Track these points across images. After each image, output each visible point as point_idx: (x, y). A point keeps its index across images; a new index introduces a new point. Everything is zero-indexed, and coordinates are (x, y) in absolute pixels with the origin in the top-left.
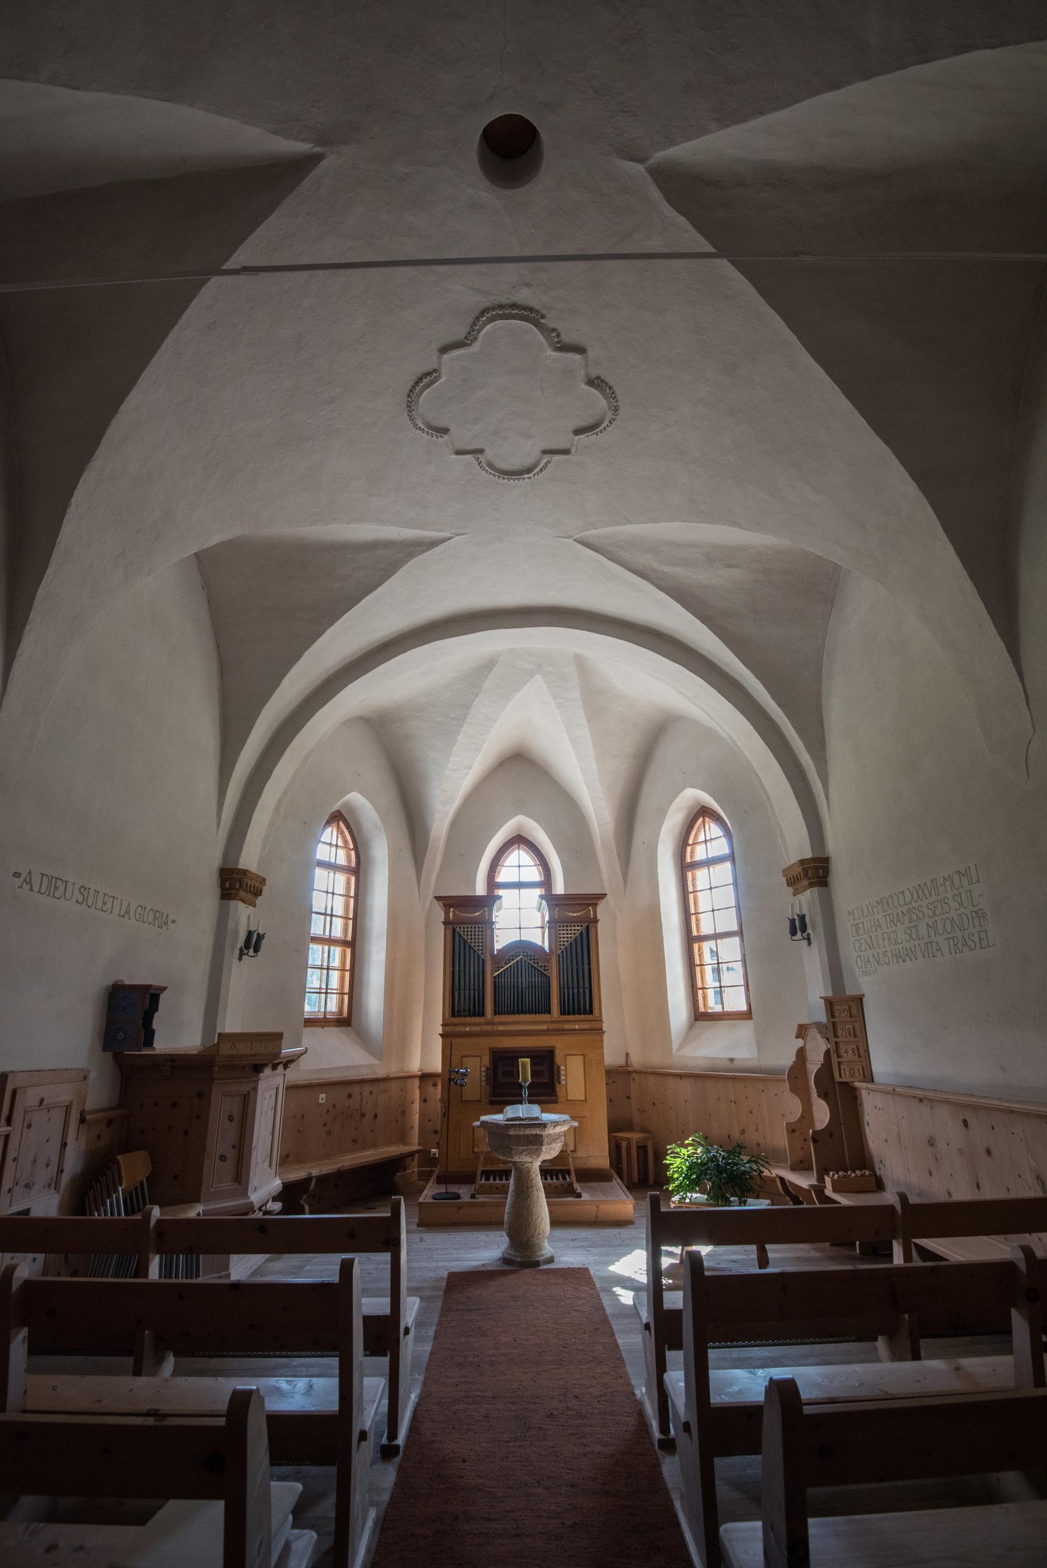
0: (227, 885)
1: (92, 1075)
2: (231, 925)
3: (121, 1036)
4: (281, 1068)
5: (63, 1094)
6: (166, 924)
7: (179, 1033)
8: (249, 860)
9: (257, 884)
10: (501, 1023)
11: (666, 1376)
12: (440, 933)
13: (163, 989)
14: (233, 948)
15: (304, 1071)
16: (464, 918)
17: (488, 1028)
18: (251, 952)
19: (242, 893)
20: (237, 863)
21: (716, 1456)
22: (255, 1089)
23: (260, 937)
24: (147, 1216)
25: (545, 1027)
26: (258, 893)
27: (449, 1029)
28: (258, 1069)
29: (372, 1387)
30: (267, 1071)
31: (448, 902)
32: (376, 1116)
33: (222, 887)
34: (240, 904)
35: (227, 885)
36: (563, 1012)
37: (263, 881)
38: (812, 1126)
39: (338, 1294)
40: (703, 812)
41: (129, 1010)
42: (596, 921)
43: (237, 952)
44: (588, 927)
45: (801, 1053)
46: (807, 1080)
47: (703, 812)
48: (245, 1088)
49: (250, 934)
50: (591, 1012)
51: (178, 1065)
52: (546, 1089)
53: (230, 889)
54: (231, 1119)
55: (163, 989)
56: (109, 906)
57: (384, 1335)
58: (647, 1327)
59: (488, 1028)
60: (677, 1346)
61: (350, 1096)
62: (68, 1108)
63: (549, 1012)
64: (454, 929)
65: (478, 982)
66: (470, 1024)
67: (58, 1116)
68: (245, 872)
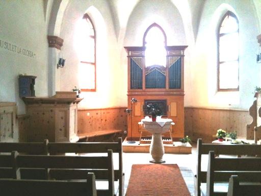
0: (51, 42)
1: (18, 104)
2: (53, 56)
3: (24, 92)
4: (76, 103)
5: (11, 109)
6: (32, 55)
7: (41, 91)
8: (57, 32)
9: (61, 42)
10: (147, 92)
11: (201, 187)
12: (126, 59)
13: (36, 77)
14: (55, 64)
15: (82, 105)
16: (134, 54)
17: (143, 93)
18: (61, 66)
19: (56, 45)
20: (53, 33)
21: (183, 104)
22: (69, 109)
23: (64, 61)
24: (45, 142)
25: (163, 93)
26: (61, 45)
27: (130, 93)
28: (69, 103)
29: (116, 184)
30: (72, 104)
31: (129, 49)
32: (106, 120)
33: (49, 43)
34: (56, 49)
35: (51, 42)
36: (170, 88)
37: (63, 40)
38: (256, 126)
39: (108, 161)
40: (229, 13)
41: (26, 84)
42: (184, 56)
43: (56, 66)
44: (180, 58)
45: (255, 103)
46: (256, 111)
47: (229, 13)
48: (66, 109)
49: (60, 59)
50: (180, 88)
51: (43, 101)
52: (164, 113)
53: (52, 43)
54: (62, 118)
55: (36, 77)
56: (14, 49)
57: (119, 175)
58: (196, 176)
59: (143, 93)
60: (205, 181)
61: (97, 114)
62: (12, 113)
63: (165, 88)
64: (131, 59)
65: (139, 78)
66: (138, 92)
67: (10, 116)
68: (56, 37)
